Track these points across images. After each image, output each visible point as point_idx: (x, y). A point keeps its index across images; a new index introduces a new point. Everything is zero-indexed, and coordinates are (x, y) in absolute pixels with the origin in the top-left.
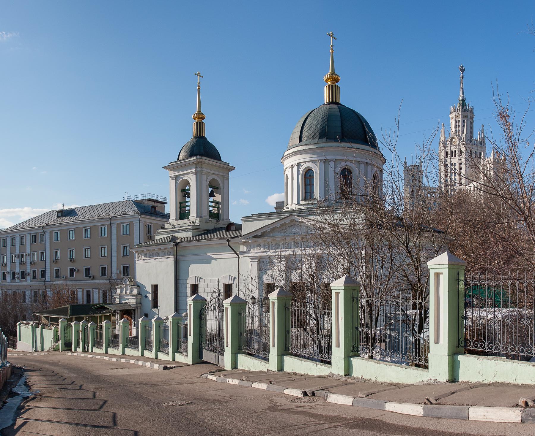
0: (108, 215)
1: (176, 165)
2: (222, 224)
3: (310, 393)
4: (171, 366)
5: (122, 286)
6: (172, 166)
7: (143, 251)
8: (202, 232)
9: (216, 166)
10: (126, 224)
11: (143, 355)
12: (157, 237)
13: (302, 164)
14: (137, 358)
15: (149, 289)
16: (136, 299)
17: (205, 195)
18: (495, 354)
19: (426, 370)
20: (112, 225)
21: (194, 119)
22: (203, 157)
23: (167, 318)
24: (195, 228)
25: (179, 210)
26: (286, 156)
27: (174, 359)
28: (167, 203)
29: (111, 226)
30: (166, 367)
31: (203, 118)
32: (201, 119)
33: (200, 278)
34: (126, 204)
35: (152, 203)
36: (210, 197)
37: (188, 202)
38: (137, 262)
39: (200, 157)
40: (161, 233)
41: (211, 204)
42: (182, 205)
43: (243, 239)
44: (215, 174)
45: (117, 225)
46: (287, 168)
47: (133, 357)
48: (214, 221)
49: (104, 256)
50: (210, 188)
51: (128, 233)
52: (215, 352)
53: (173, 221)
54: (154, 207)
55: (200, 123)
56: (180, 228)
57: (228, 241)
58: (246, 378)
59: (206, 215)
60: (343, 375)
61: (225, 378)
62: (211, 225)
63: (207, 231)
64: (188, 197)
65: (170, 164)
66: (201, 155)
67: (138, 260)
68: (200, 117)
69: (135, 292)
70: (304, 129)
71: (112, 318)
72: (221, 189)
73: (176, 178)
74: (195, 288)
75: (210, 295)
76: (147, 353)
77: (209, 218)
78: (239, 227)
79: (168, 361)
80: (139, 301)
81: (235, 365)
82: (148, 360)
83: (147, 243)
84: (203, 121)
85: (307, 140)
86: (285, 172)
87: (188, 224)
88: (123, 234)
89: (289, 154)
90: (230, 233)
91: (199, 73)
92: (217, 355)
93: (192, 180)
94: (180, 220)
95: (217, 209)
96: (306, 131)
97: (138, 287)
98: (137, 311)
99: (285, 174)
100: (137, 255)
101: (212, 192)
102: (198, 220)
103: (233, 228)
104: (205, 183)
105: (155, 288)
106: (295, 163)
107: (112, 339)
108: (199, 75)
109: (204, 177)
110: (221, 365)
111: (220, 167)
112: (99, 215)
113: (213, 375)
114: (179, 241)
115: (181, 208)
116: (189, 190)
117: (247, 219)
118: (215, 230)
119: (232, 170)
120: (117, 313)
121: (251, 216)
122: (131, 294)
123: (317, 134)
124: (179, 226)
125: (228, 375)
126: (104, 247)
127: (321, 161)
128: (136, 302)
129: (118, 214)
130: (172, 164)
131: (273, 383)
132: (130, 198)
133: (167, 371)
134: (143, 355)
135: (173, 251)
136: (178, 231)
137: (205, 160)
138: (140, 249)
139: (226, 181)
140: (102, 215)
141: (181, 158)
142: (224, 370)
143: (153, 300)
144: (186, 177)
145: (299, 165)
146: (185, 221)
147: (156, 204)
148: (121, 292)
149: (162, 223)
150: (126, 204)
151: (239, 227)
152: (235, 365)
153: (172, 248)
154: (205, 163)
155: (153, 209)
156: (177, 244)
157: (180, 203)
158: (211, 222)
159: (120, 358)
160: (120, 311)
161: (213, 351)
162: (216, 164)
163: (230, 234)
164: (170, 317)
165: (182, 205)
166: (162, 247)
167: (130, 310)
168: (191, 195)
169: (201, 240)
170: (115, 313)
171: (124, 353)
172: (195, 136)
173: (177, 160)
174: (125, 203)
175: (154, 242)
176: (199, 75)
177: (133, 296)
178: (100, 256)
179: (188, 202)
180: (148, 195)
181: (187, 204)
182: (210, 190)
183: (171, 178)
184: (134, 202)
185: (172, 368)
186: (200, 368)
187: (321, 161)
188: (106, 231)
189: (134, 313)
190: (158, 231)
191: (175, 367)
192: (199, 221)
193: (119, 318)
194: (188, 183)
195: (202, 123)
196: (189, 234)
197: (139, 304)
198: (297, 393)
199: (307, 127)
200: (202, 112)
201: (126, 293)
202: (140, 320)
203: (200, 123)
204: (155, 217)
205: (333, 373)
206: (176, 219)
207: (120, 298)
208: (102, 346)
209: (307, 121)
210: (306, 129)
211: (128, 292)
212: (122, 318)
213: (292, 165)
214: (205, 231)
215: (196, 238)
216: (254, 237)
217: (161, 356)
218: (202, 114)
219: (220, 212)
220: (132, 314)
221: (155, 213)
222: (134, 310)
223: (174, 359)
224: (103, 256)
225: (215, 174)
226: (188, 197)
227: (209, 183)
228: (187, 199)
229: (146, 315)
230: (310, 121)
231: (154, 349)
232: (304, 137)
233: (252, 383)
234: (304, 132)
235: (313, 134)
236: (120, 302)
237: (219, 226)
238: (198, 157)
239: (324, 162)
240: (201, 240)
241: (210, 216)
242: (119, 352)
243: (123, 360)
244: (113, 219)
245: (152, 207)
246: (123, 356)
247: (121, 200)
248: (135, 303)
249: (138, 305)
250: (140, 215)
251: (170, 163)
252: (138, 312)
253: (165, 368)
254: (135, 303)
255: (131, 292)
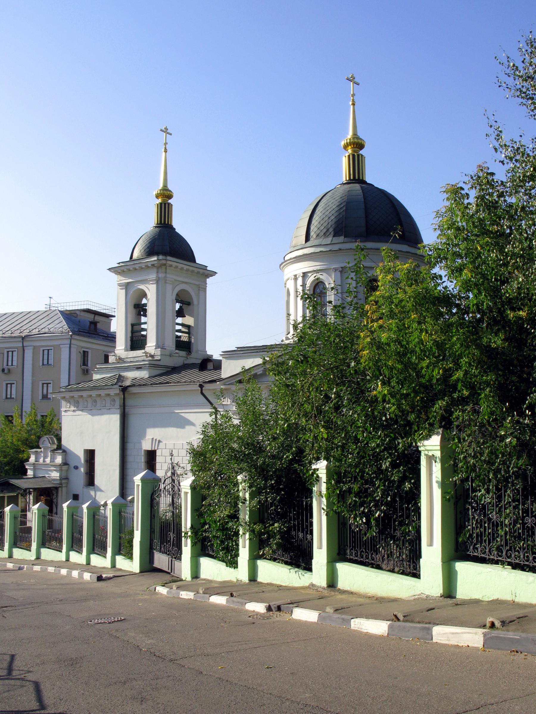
0: (19, 331)
1: (128, 267)
2: (195, 358)
3: (275, 608)
4: (109, 575)
5: (39, 450)
6: (122, 268)
7: (73, 397)
8: (164, 370)
9: (187, 270)
10: (48, 348)
11: (68, 560)
12: (96, 377)
13: (310, 275)
14: (58, 565)
15: (81, 455)
16: (61, 471)
17: (170, 314)
18: (497, 562)
19: (309, 573)
20: (25, 348)
21: (157, 197)
22: (169, 258)
23: (105, 505)
24: (153, 364)
25: (129, 335)
26: (286, 261)
27: (114, 565)
28: (114, 316)
29: (24, 350)
30: (101, 576)
31: (170, 197)
32: (167, 198)
33: (159, 441)
34: (50, 316)
35: (91, 317)
36: (178, 316)
37: (145, 323)
38: (63, 413)
39: (164, 257)
40: (100, 371)
41: (178, 327)
42: (136, 328)
43: (222, 385)
44: (186, 283)
45: (34, 349)
46: (288, 279)
47: (51, 563)
48: (183, 353)
49: (11, 398)
50: (177, 304)
51: (51, 362)
52: (168, 555)
53: (150, 348)
54: (94, 323)
55: (165, 204)
56: (131, 364)
57: (201, 386)
58: (204, 590)
59: (171, 344)
60: (326, 586)
61: (179, 591)
62: (179, 358)
63: (172, 369)
64: (145, 315)
65: (119, 265)
66: (165, 254)
67: (66, 411)
68: (166, 196)
69: (59, 460)
70: (313, 222)
71: (20, 499)
72: (193, 304)
73: (127, 286)
74: (151, 456)
75: (164, 474)
76: (75, 557)
77: (174, 349)
78: (218, 365)
79: (104, 568)
80: (64, 475)
81: (196, 575)
82: (76, 566)
83: (80, 386)
84: (170, 201)
85: (316, 239)
86: (285, 284)
87: (142, 358)
88: (43, 364)
89: (291, 259)
90: (205, 373)
91: (166, 129)
92: (170, 559)
93: (151, 290)
94: (132, 350)
95: (187, 335)
96: (315, 225)
97: (64, 453)
98: (62, 490)
99: (285, 287)
100: (63, 403)
101: (181, 308)
102: (158, 352)
103: (210, 366)
104: (171, 296)
105: (90, 455)
106: (300, 273)
107: (19, 534)
108: (165, 131)
109: (169, 287)
110: (176, 573)
111: (193, 271)
112: (4, 332)
113: (163, 587)
114: (127, 383)
115: (133, 332)
116: (145, 305)
117: (230, 355)
118: (185, 367)
119: (212, 276)
120: (30, 493)
121: (235, 351)
122: (52, 464)
123: (331, 230)
124: (129, 360)
125: (186, 587)
126: (11, 384)
127: (335, 270)
128: (60, 476)
129: (35, 331)
130: (121, 264)
131: (235, 595)
132: (56, 305)
133: (101, 584)
134: (68, 560)
135: (118, 402)
136: (128, 369)
137: (172, 261)
138: (68, 395)
139: (201, 293)
140: (10, 332)
141: (135, 256)
142: (182, 580)
143: (86, 473)
144: (142, 287)
145: (305, 275)
146: (139, 353)
147: (98, 318)
148: (37, 460)
149: (106, 349)
150: (50, 316)
151: (218, 365)
152: (196, 575)
153: (118, 394)
154: (171, 266)
155: (93, 326)
156: (124, 389)
157: (133, 325)
158: (177, 355)
159: (33, 565)
160: (35, 489)
161: (167, 553)
162: (188, 267)
163: (207, 376)
164: (109, 502)
165: (136, 328)
166: (103, 393)
167: (50, 488)
168: (149, 313)
169: (160, 383)
170: (26, 492)
171: (38, 557)
172: (158, 224)
173: (128, 259)
174: (48, 313)
175: (91, 384)
176: (165, 131)
177: (55, 466)
178: (4, 397)
179: (145, 323)
180: (85, 303)
181: (143, 326)
182: (178, 306)
183: (120, 286)
184: (61, 312)
185: (110, 578)
186: (150, 579)
187: (335, 270)
188: (15, 358)
189: (57, 493)
190: (98, 367)
191: (115, 577)
192: (159, 353)
193: (32, 501)
194: (144, 295)
195: (169, 204)
196: (144, 374)
197: (65, 479)
198: (259, 608)
199: (316, 219)
200: (170, 187)
201: (44, 461)
202: (65, 505)
203: (165, 204)
204: (94, 338)
205: (314, 583)
206: (126, 350)
207: (34, 470)
208: (4, 546)
209: (317, 211)
210: (315, 222)
211: (48, 460)
212: (36, 502)
213: (295, 276)
214: (169, 369)
215: (155, 380)
216: (240, 382)
217: (97, 560)
218: (168, 190)
219: (193, 341)
220: (53, 495)
221: (95, 333)
222: (57, 488)
223: (114, 565)
224: (9, 399)
225: (186, 283)
226: (145, 315)
227: (177, 295)
228: (143, 319)
229: (76, 497)
230: (321, 211)
231: (85, 549)
232: (312, 234)
233: (210, 596)
234: (312, 228)
235: (325, 230)
236: (34, 475)
237: (191, 361)
238: (161, 257)
239: (341, 272)
240: (160, 383)
241: (176, 345)
242: (31, 555)
243: (37, 568)
244: (27, 339)
245: (91, 323)
246: (37, 562)
247: (43, 308)
248: (58, 478)
249: (64, 481)
250: (71, 336)
251: (119, 263)
252: (62, 492)
253: (100, 579)
254: (58, 478)
255: (53, 460)
